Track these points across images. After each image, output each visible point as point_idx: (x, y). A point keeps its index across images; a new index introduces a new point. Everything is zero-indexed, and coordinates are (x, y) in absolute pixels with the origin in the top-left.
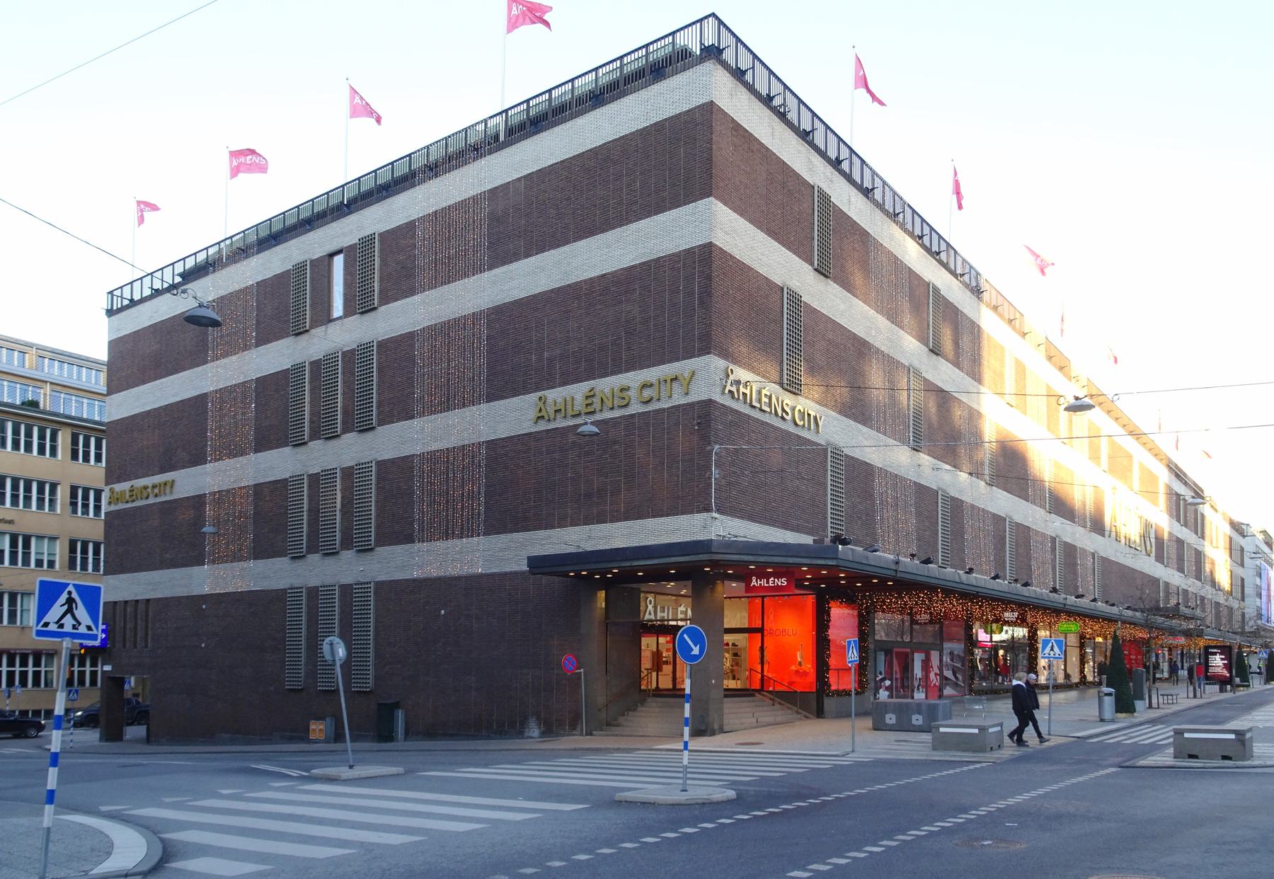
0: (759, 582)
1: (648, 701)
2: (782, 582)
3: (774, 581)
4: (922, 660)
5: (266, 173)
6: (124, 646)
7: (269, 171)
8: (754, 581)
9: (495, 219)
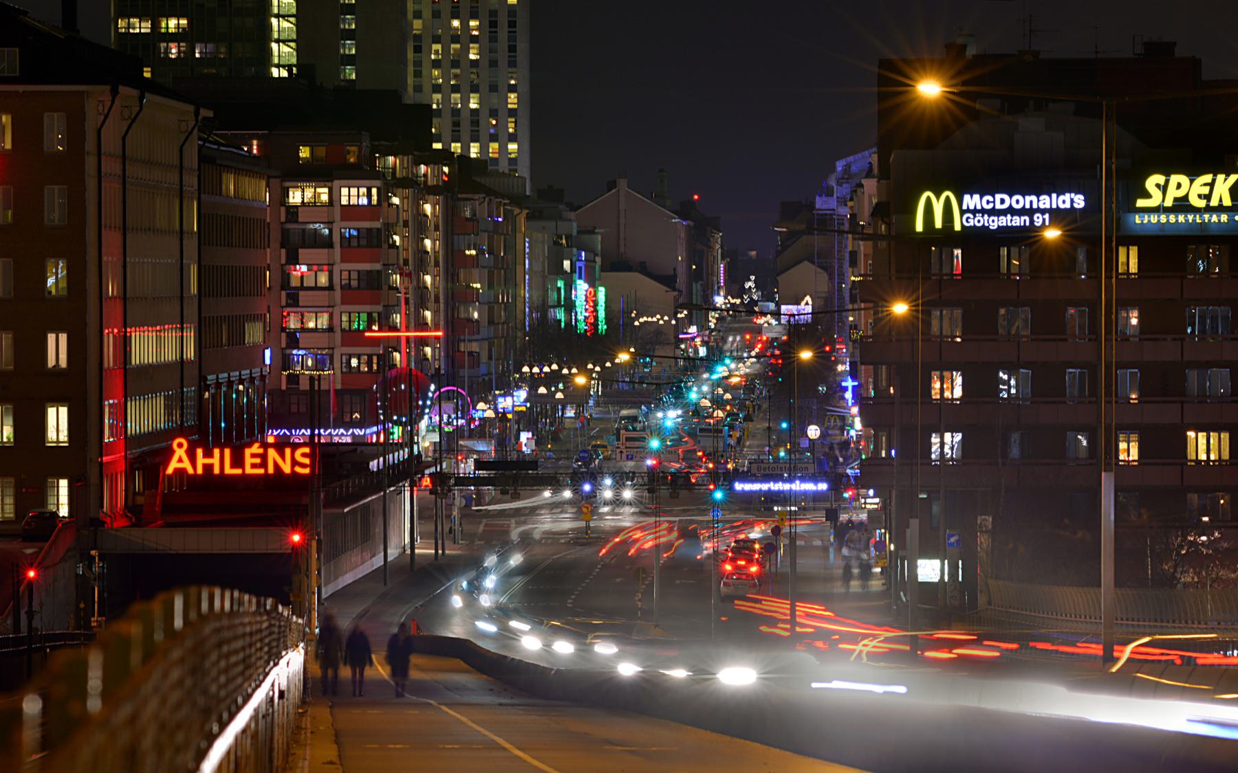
0: (201, 460)
2: (295, 463)
3: (264, 457)
6: (581, 452)
8: (180, 453)
9: (297, 525)
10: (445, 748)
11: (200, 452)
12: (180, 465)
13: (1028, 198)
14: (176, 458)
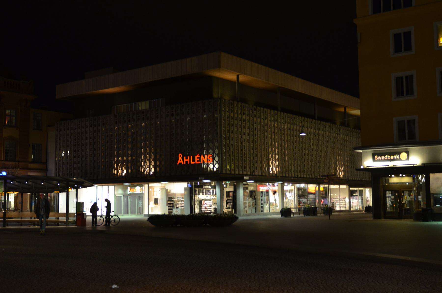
0: (185, 160)
1: (382, 219)
3: (200, 158)
4: (165, 214)
5: (83, 203)
7: (184, 188)
8: (180, 158)
10: (7, 202)
11: (185, 158)
12: (181, 162)
13: (394, 156)
14: (179, 160)
